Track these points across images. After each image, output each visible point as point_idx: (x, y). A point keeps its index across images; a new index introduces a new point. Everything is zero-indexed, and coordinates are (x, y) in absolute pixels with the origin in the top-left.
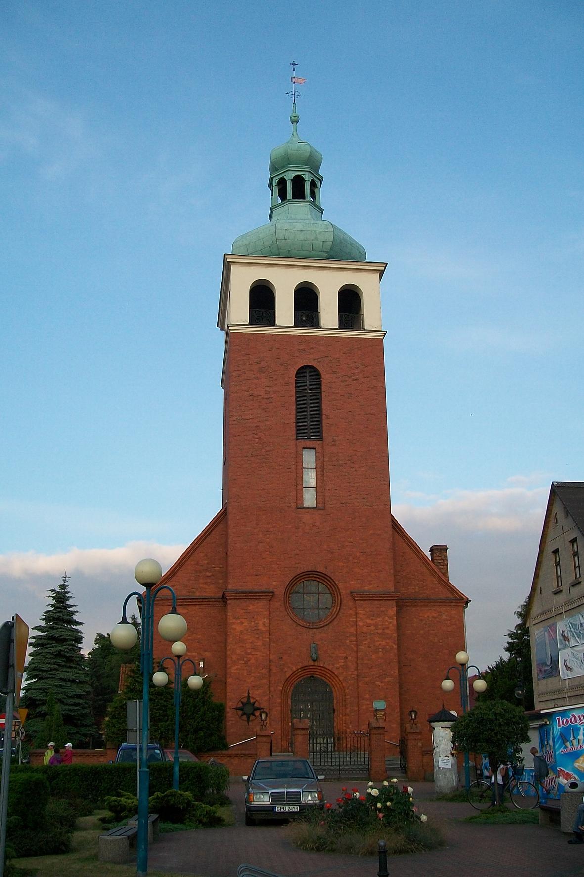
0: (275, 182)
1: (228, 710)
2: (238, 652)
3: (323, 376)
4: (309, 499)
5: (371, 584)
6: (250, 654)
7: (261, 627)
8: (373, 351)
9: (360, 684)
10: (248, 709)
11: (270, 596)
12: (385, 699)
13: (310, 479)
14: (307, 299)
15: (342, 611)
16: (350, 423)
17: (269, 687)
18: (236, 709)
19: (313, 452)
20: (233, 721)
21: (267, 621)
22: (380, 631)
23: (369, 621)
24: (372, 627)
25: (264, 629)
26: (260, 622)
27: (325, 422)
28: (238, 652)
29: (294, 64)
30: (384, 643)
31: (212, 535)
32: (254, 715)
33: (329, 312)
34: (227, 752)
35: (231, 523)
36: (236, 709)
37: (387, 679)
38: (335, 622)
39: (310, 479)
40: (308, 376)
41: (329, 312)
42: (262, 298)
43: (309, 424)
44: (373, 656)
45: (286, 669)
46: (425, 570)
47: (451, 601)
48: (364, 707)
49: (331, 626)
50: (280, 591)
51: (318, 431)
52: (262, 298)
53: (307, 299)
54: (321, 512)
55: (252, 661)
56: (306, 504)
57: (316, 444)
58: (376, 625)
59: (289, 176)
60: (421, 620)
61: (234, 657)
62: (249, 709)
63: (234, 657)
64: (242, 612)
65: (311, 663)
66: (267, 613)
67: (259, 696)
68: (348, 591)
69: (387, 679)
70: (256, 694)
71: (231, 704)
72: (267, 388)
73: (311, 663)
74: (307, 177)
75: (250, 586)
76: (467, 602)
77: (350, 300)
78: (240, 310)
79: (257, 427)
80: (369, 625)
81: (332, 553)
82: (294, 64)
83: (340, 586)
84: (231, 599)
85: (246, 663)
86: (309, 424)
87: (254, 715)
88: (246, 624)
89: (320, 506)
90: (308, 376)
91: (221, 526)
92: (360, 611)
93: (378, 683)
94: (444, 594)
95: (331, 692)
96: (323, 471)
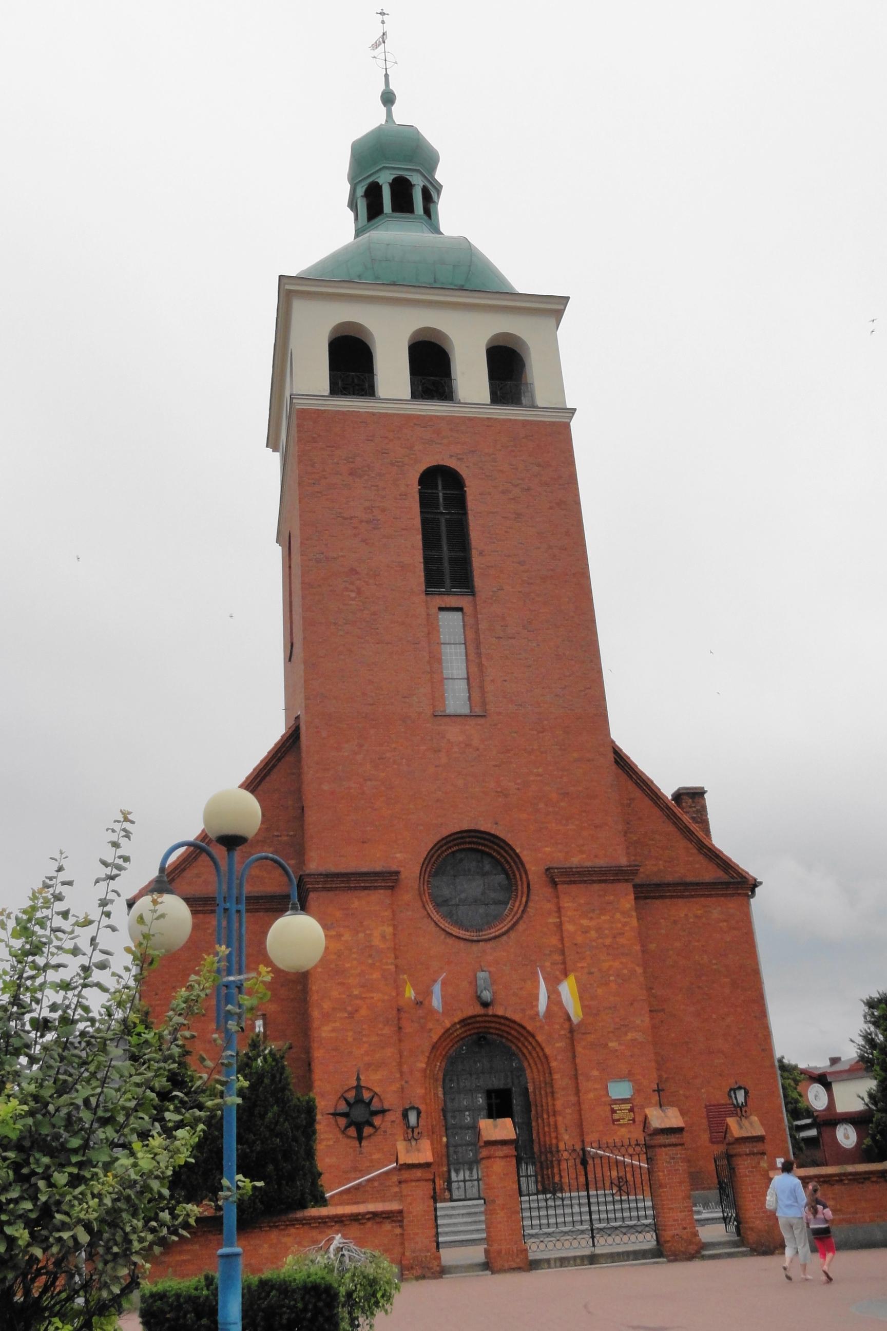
0: (361, 191)
1: (319, 1117)
2: (335, 994)
3: (467, 483)
4: (456, 698)
5: (582, 852)
6: (357, 997)
7: (376, 941)
8: (551, 445)
9: (116, 1290)
10: (359, 1113)
11: (387, 880)
12: (629, 1076)
13: (455, 663)
14: (430, 364)
15: (530, 904)
16: (522, 563)
17: (400, 1064)
18: (335, 1114)
19: (458, 616)
20: (330, 1147)
21: (389, 930)
22: (608, 941)
23: (585, 922)
24: (593, 934)
25: (382, 946)
26: (376, 934)
27: (477, 562)
28: (335, 994)
29: (382, 14)
30: (616, 964)
31: (274, 775)
32: (371, 1125)
33: (471, 378)
34: (324, 1211)
35: (310, 773)
36: (335, 1114)
37: (630, 1036)
38: (521, 927)
39: (455, 663)
40: (442, 489)
41: (471, 378)
42: (351, 360)
43: (448, 563)
44: (600, 991)
45: (430, 1025)
46: (671, 828)
47: (727, 885)
48: (591, 1095)
49: (513, 934)
50: (411, 871)
51: (463, 579)
52: (351, 360)
53: (430, 364)
54: (481, 721)
55: (363, 1012)
56: (450, 710)
57: (463, 601)
58: (599, 929)
59: (385, 180)
60: (675, 922)
61: (326, 1005)
62: (360, 1115)
63: (326, 1005)
64: (339, 914)
65: (479, 1010)
66: (388, 913)
67: (383, 1085)
68: (542, 868)
69: (630, 1036)
70: (373, 1080)
71: (326, 1096)
72: (368, 504)
73: (479, 1010)
74: (418, 182)
75: (350, 863)
76: (755, 885)
77: (507, 367)
78: (314, 375)
79: (353, 571)
80: (586, 931)
81: (506, 796)
82: (382, 14)
83: (526, 856)
84: (315, 890)
85: (351, 1015)
86: (448, 563)
87: (371, 1125)
88: (347, 937)
89: (478, 711)
90: (442, 489)
91: (290, 758)
92: (566, 903)
93: (613, 1045)
94: (710, 874)
95: (521, 1069)
96: (478, 647)
